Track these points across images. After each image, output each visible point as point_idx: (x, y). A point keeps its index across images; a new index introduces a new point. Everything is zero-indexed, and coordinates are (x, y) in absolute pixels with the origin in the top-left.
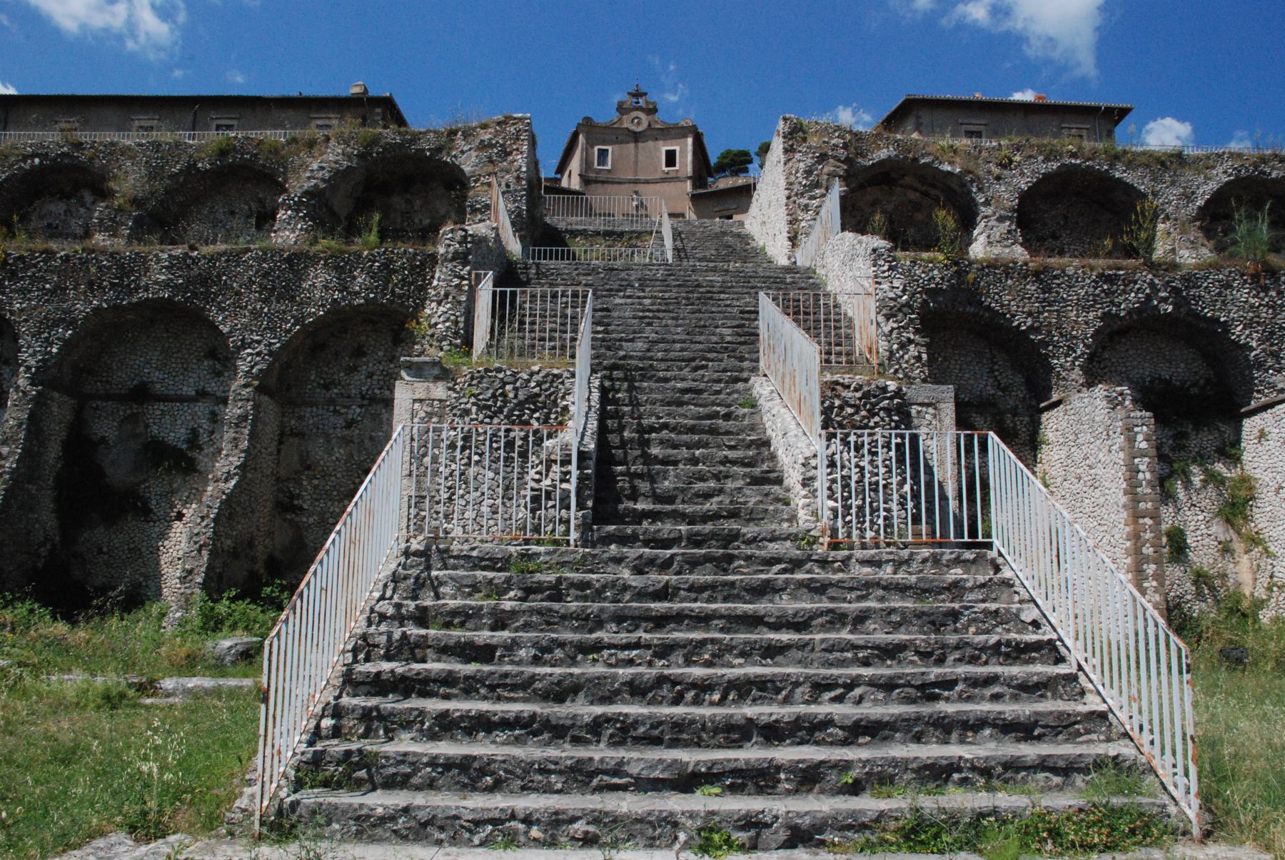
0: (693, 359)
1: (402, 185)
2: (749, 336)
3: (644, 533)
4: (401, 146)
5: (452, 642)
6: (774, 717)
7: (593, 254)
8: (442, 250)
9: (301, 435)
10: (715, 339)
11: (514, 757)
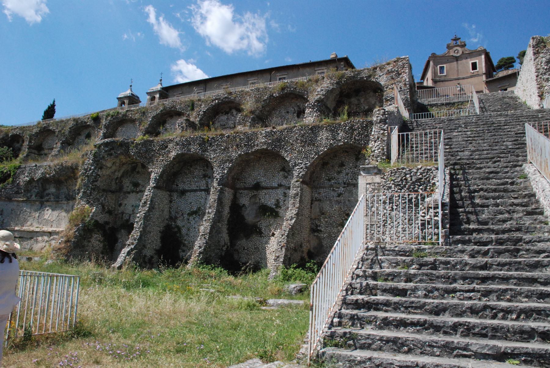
0: (493, 158)
1: (356, 93)
2: (520, 145)
3: (474, 239)
4: (354, 77)
5: (388, 287)
6: (546, 329)
7: (441, 114)
8: (375, 119)
9: (320, 200)
10: (503, 147)
11: (417, 339)
